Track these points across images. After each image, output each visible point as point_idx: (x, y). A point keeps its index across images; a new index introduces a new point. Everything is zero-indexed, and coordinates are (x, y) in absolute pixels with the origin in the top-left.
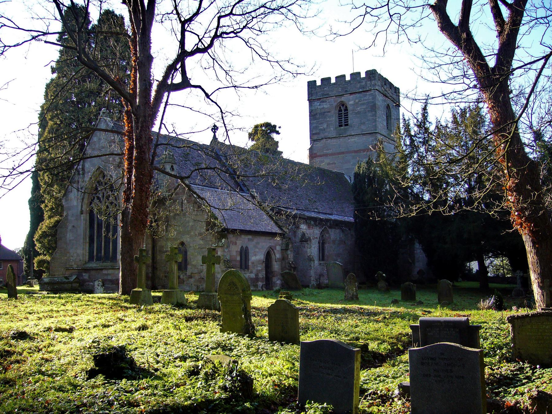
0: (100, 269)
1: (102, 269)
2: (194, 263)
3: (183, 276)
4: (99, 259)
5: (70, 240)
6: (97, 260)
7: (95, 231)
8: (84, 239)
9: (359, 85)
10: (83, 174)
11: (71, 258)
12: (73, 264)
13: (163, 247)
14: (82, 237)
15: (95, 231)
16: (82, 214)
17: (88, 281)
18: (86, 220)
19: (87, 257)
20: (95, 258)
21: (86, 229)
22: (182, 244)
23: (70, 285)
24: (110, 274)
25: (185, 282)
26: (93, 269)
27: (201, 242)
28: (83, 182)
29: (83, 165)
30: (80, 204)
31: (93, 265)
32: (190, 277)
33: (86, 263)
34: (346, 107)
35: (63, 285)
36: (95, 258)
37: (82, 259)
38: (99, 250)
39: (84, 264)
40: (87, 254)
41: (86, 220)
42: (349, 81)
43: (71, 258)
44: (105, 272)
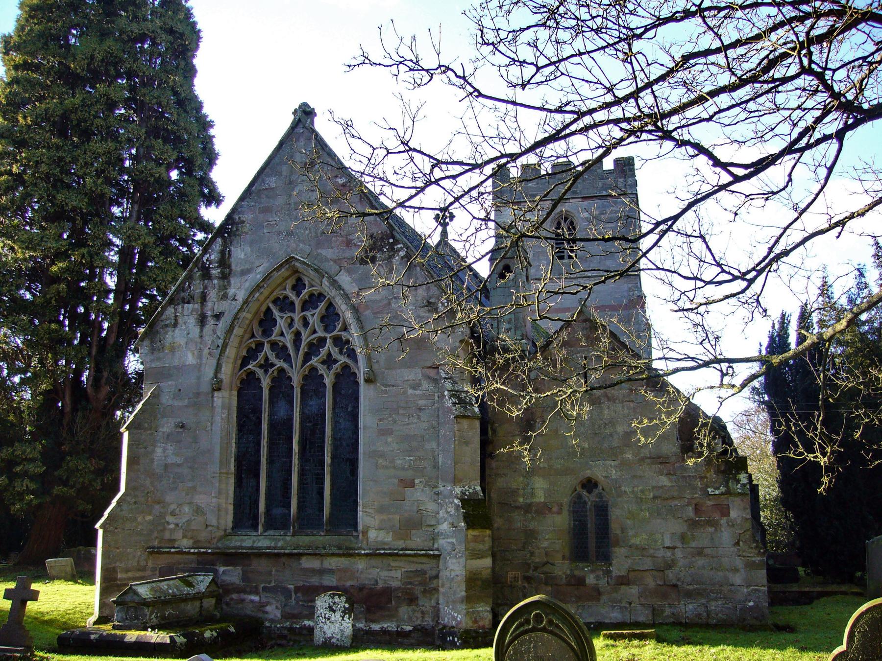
0: (291, 555)
1: (300, 555)
2: (637, 541)
3: (598, 578)
4: (276, 523)
5: (166, 466)
6: (269, 526)
7: (264, 442)
8: (223, 463)
9: (600, 184)
10: (225, 277)
11: (169, 518)
12: (178, 535)
13: (514, 492)
14: (217, 455)
15: (264, 442)
16: (219, 389)
17: (239, 590)
18: (229, 409)
19: (230, 518)
20: (262, 519)
21: (229, 433)
22: (590, 484)
23: (197, 604)
24: (331, 571)
25: (604, 598)
26: (260, 555)
27: (664, 481)
28: (224, 297)
29: (222, 253)
30: (214, 362)
31: (248, 541)
32: (624, 581)
33: (226, 535)
34: (572, 223)
35: (183, 605)
36: (262, 519)
37: (214, 522)
38: (279, 493)
39: (221, 539)
40: (231, 508)
41: (229, 409)
42: (609, 172)
43: (169, 518)
44: (308, 563)
